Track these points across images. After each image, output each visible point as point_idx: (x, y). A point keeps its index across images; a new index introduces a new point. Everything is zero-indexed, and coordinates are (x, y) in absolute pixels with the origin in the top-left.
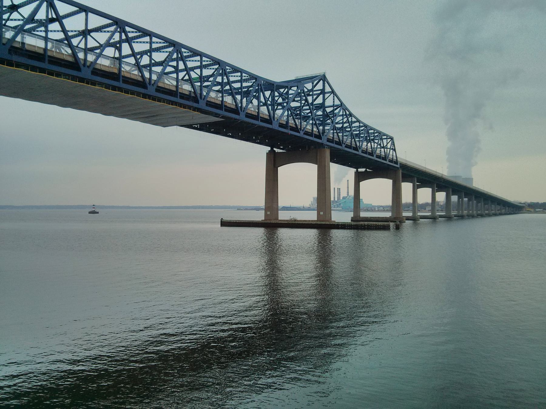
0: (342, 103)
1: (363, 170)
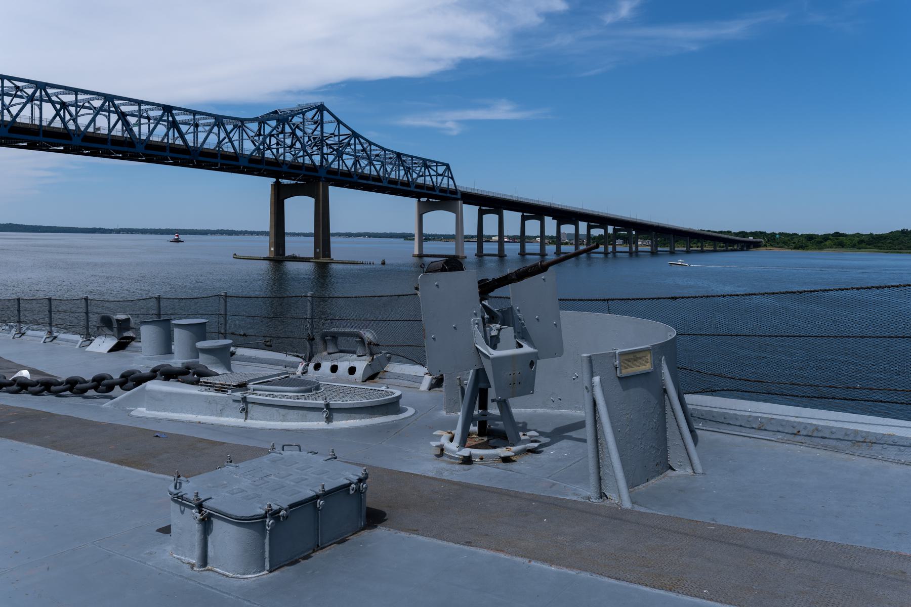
0: (353, 132)
1: (425, 200)
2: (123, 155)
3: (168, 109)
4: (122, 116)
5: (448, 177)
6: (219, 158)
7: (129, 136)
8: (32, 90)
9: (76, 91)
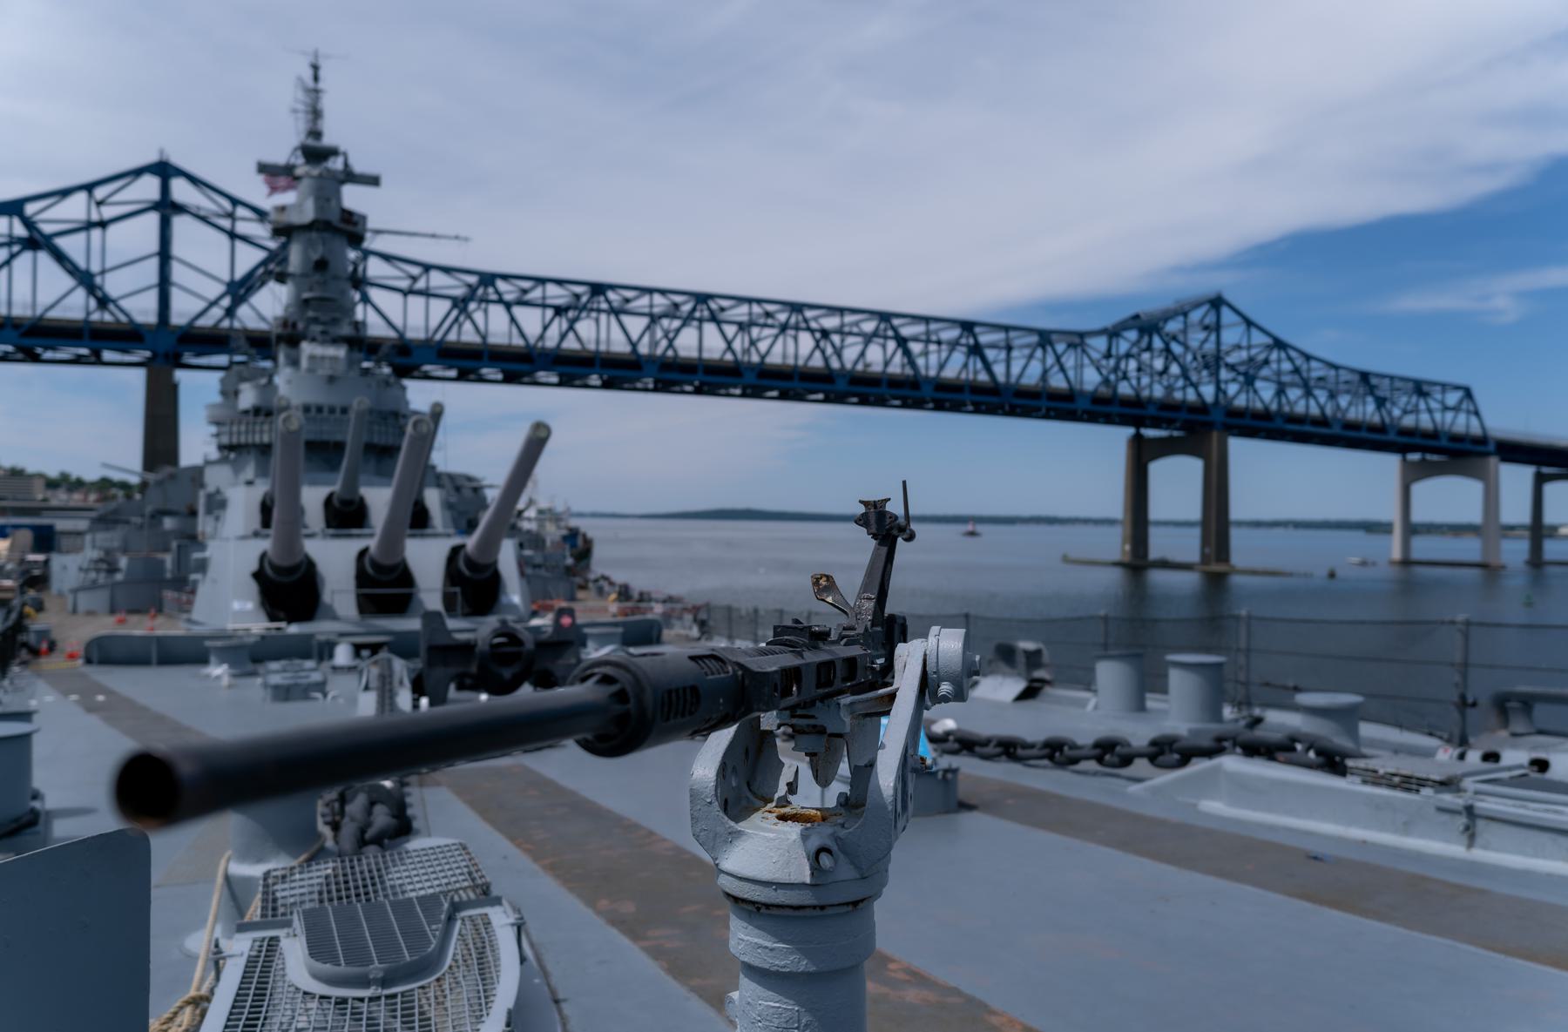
3: (885, 317)
4: (902, 342)
5: (1468, 412)
9: (841, 311)
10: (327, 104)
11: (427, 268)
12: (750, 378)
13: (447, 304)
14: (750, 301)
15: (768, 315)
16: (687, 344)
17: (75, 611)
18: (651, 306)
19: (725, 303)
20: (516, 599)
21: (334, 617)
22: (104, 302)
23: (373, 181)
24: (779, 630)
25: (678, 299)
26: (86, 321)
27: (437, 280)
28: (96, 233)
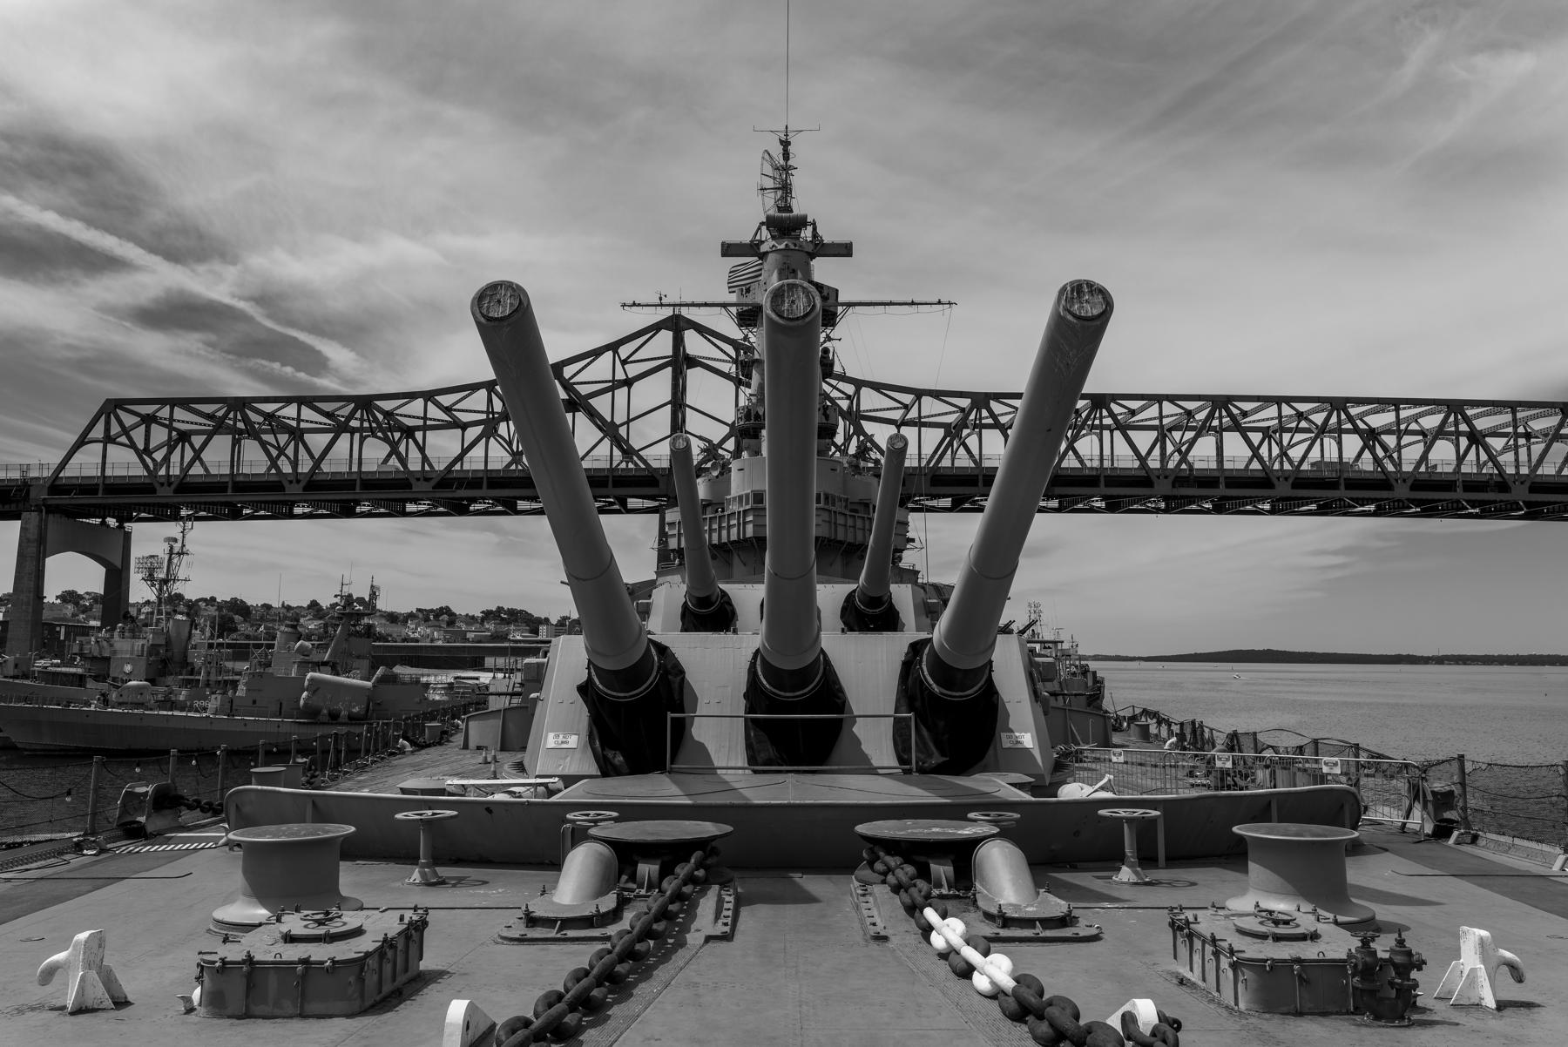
2: (1482, 511)
3: (1455, 407)
4: (1476, 438)
6: (1342, 487)
7: (1496, 472)
8: (1324, 414)
9: (1396, 404)
10: (797, 180)
11: (919, 394)
12: (1284, 489)
13: (941, 432)
14: (1279, 401)
15: (1300, 416)
16: (1203, 453)
17: (466, 746)
18: (1161, 417)
19: (1247, 406)
20: (1028, 740)
21: (865, 767)
22: (629, 452)
23: (845, 250)
24: (404, 753)
25: (1191, 405)
26: (611, 470)
27: (930, 406)
28: (621, 393)
